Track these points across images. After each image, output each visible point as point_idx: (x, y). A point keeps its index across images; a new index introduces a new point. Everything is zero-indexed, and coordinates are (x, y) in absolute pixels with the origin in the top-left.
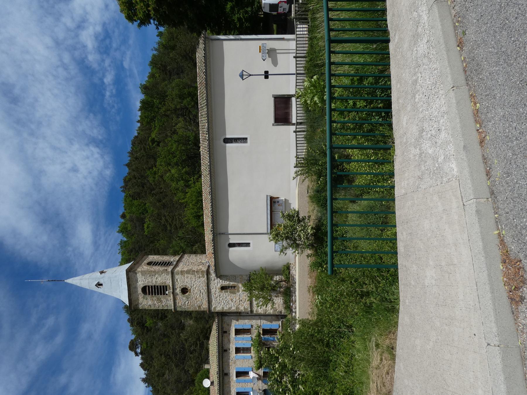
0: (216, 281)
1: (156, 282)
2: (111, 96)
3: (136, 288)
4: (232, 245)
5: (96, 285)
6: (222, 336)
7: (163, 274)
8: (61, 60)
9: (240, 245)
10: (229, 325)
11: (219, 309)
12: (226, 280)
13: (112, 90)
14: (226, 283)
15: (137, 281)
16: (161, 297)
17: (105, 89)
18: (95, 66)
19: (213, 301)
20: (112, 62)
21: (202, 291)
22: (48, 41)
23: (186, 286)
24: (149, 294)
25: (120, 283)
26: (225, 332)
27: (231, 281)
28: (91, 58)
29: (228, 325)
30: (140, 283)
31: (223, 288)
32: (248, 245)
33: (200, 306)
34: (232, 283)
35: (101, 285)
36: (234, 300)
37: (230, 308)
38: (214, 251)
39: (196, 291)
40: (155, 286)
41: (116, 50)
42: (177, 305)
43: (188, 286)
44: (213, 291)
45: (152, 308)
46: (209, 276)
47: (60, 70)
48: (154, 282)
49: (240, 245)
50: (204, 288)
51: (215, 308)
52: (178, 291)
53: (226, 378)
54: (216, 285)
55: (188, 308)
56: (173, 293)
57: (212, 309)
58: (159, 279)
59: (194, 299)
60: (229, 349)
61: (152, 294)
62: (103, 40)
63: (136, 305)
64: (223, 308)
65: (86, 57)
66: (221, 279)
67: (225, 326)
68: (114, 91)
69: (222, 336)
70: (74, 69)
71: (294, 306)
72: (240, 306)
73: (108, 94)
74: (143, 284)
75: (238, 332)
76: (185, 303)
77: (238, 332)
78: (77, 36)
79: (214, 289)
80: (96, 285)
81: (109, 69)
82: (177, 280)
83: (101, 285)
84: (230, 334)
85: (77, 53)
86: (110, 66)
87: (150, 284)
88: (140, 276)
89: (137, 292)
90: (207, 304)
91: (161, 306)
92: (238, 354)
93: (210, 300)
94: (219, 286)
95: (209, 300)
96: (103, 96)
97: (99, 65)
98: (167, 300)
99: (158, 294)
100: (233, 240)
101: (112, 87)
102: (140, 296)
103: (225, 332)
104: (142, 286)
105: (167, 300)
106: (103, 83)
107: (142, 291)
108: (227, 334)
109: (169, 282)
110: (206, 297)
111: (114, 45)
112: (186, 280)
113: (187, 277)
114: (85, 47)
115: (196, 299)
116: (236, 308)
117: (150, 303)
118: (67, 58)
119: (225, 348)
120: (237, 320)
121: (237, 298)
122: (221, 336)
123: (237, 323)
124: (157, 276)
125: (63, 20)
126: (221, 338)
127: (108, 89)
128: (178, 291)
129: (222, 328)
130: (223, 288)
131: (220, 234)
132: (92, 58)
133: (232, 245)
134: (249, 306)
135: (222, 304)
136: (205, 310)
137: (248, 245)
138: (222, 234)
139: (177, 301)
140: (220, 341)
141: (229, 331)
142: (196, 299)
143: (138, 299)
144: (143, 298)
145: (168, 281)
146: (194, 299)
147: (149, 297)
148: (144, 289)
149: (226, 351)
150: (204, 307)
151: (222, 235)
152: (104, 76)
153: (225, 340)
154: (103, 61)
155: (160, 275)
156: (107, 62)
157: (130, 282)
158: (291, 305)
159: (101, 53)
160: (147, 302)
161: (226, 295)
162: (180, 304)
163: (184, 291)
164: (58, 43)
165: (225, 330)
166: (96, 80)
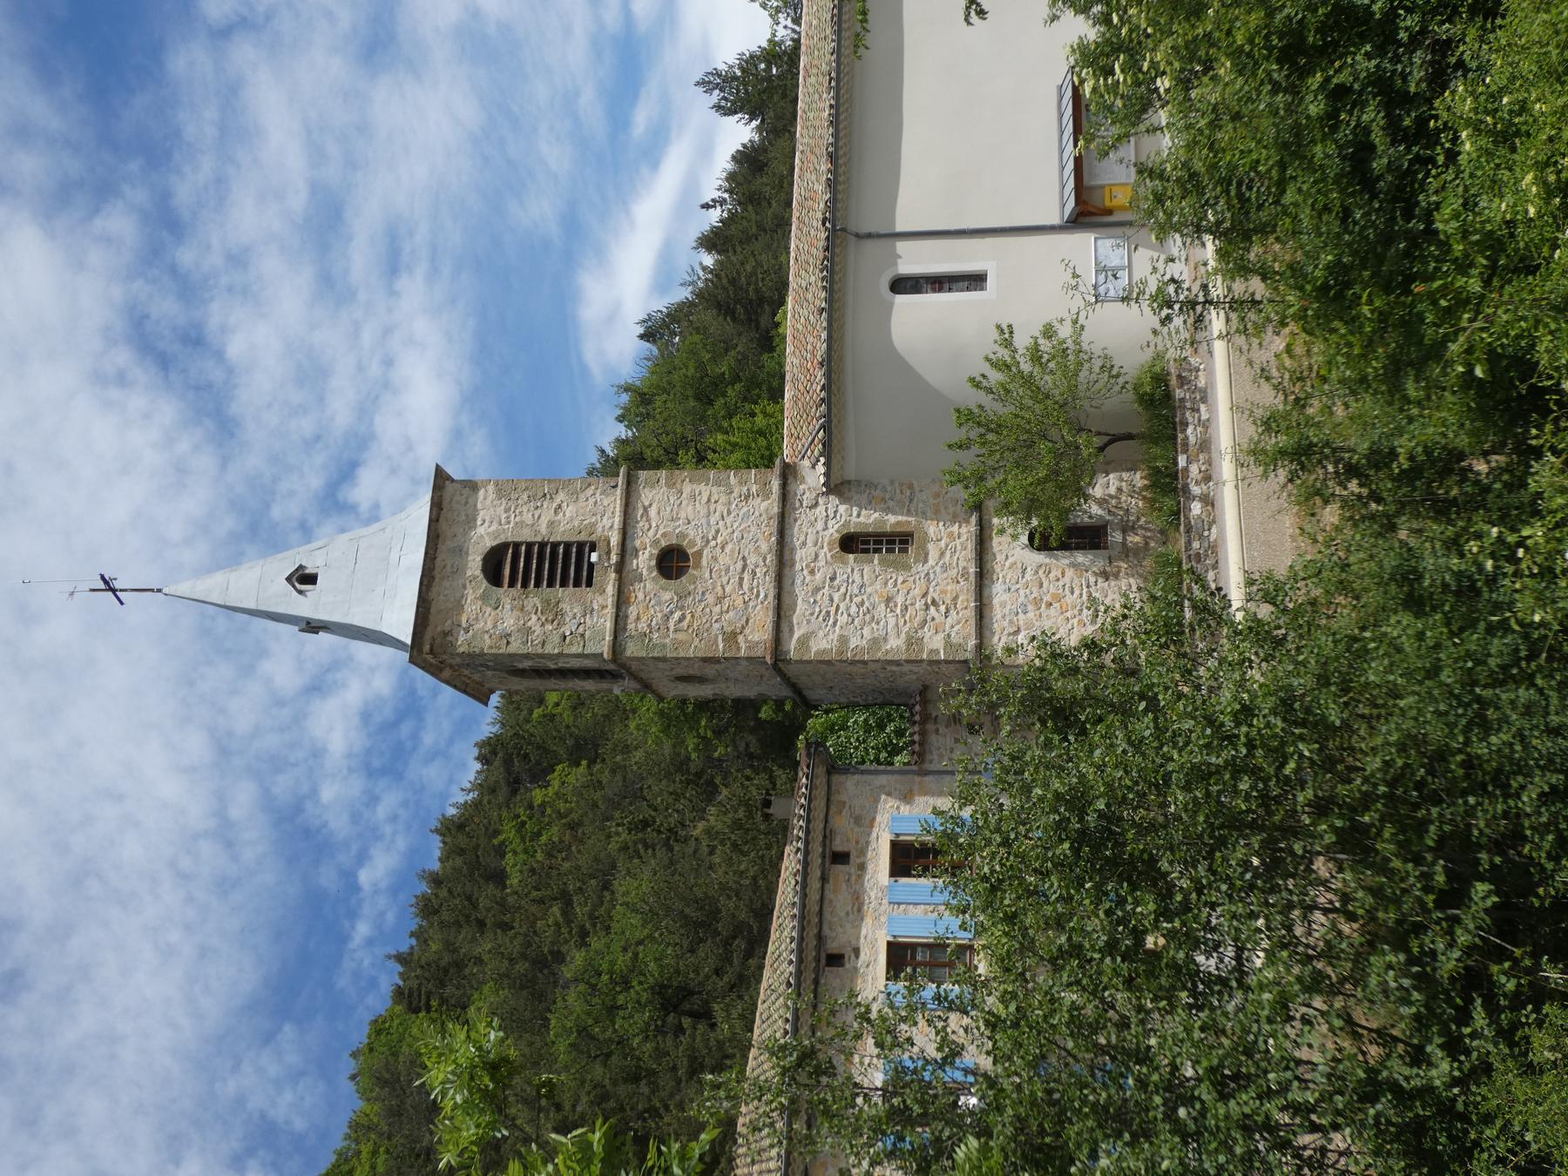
0: (820, 509)
1: (551, 524)
2: (370, 942)
3: (461, 552)
4: (902, 285)
5: (289, 579)
6: (824, 879)
7: (590, 491)
8: (220, 813)
9: (939, 283)
10: (865, 822)
11: (824, 645)
12: (870, 504)
13: (382, 914)
14: (867, 519)
15: (471, 522)
16: (567, 598)
17: (353, 915)
18: (339, 824)
19: (801, 606)
20: (405, 804)
21: (752, 560)
22: (196, 745)
23: (682, 535)
24: (512, 584)
25: (394, 556)
26: (841, 858)
27: (888, 510)
28: (328, 793)
29: (858, 820)
30: (481, 530)
31: (851, 543)
32: (976, 281)
33: (734, 635)
34: (892, 520)
35: (311, 579)
36: (900, 600)
37: (875, 642)
38: (830, 300)
39: (724, 560)
40: (542, 545)
41: (435, 755)
42: (631, 626)
43: (693, 538)
44: (802, 556)
45: (512, 649)
46: (791, 487)
47: (207, 848)
48: (543, 529)
49: (939, 283)
50: (764, 547)
51: (804, 641)
52: (644, 561)
53: (831, 977)
54: (820, 525)
55: (677, 644)
56: (620, 567)
57: (792, 647)
58: (569, 511)
59: (710, 598)
60: (857, 952)
61: (525, 585)
62: (391, 726)
63: (446, 634)
64: (843, 640)
65: (314, 793)
66: (844, 499)
67: (841, 823)
68: (390, 917)
69: (824, 879)
70: (255, 840)
71: (1194, 469)
72: (927, 633)
73: (363, 929)
74: (496, 535)
75: (907, 859)
76: (667, 617)
77: (907, 859)
78: (299, 719)
79: (810, 550)
80: (289, 579)
81: (388, 829)
82: (645, 509)
83: (311, 579)
84: (862, 867)
85: (283, 785)
86: (394, 819)
87: (526, 535)
88: (491, 496)
89: (458, 571)
90: (769, 626)
91: (556, 639)
92: (903, 880)
93: (786, 599)
94: (833, 531)
95: (779, 597)
96: (344, 939)
97: (355, 818)
98: (588, 611)
99: (550, 585)
100: (914, 260)
101: (382, 902)
102: (469, 591)
103: (841, 858)
104: (490, 543)
105: (588, 611)
106: (353, 887)
107: (485, 570)
108: (851, 868)
109: (609, 526)
110: (767, 587)
111: (428, 739)
112: (687, 510)
113: (693, 497)
114: (318, 753)
115: (720, 600)
116: (910, 642)
117: (509, 622)
118: (243, 799)
119: (833, 946)
120: (907, 798)
121: (917, 592)
122: (816, 873)
123: (905, 810)
124: (561, 496)
125: (266, 667)
126: (815, 884)
127: (367, 909)
128: (644, 561)
129: (828, 836)
130: (851, 543)
131: (857, 235)
132: (335, 794)
133: (902, 285)
134: (971, 628)
135: (843, 619)
136: (759, 652)
137: (976, 281)
138: (869, 236)
139: (633, 611)
140: (814, 896)
141: (863, 852)
142: (720, 600)
143: (459, 607)
144: (484, 598)
145: (606, 522)
146: (710, 598)
147: (506, 595)
148: (495, 565)
149: (836, 960)
150: (755, 637)
151: (869, 245)
152: (362, 858)
153: (839, 900)
154: (373, 800)
155: (575, 496)
156: (390, 800)
157: (443, 525)
158: (1182, 461)
159: (371, 773)
160: (496, 621)
161: (867, 573)
162: (643, 626)
163: (673, 562)
164: (224, 748)
165: (839, 846)
166: (328, 878)
